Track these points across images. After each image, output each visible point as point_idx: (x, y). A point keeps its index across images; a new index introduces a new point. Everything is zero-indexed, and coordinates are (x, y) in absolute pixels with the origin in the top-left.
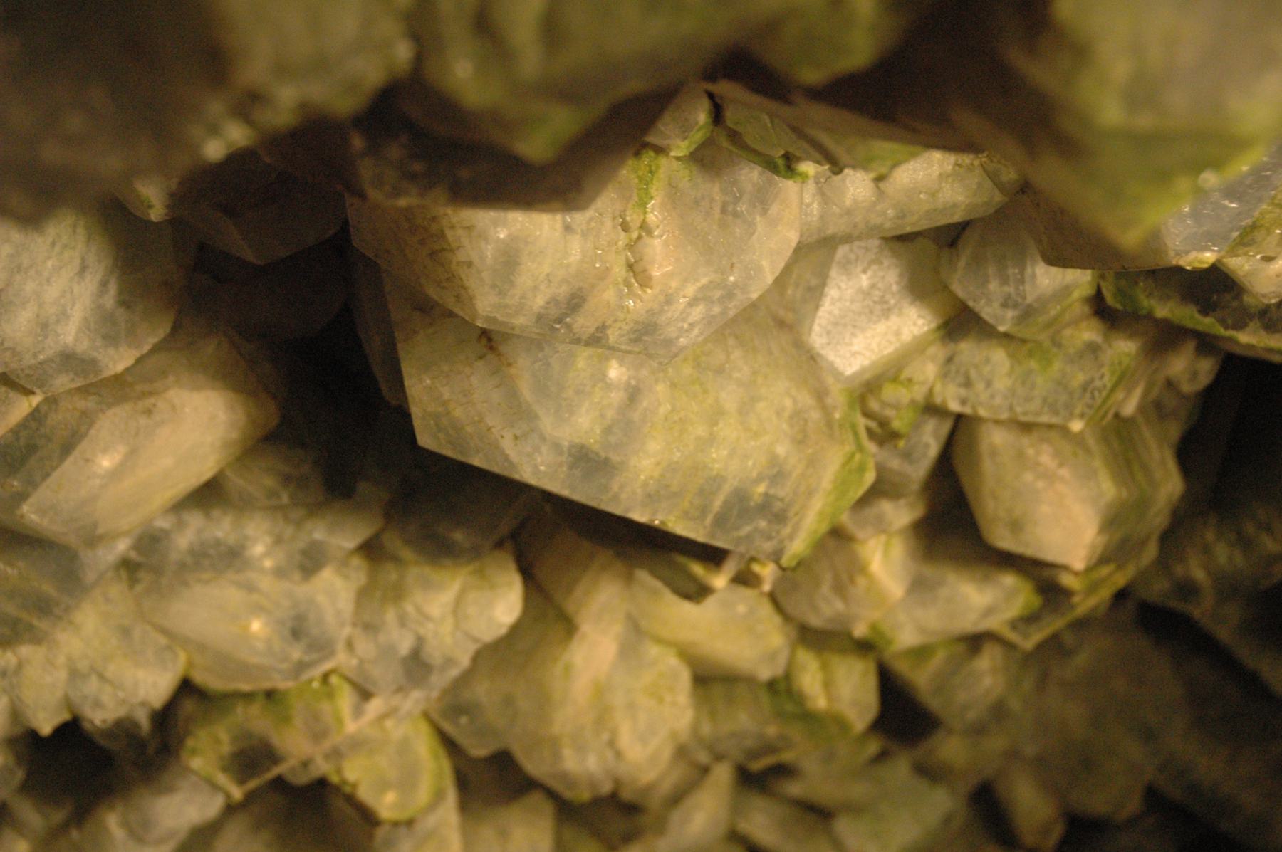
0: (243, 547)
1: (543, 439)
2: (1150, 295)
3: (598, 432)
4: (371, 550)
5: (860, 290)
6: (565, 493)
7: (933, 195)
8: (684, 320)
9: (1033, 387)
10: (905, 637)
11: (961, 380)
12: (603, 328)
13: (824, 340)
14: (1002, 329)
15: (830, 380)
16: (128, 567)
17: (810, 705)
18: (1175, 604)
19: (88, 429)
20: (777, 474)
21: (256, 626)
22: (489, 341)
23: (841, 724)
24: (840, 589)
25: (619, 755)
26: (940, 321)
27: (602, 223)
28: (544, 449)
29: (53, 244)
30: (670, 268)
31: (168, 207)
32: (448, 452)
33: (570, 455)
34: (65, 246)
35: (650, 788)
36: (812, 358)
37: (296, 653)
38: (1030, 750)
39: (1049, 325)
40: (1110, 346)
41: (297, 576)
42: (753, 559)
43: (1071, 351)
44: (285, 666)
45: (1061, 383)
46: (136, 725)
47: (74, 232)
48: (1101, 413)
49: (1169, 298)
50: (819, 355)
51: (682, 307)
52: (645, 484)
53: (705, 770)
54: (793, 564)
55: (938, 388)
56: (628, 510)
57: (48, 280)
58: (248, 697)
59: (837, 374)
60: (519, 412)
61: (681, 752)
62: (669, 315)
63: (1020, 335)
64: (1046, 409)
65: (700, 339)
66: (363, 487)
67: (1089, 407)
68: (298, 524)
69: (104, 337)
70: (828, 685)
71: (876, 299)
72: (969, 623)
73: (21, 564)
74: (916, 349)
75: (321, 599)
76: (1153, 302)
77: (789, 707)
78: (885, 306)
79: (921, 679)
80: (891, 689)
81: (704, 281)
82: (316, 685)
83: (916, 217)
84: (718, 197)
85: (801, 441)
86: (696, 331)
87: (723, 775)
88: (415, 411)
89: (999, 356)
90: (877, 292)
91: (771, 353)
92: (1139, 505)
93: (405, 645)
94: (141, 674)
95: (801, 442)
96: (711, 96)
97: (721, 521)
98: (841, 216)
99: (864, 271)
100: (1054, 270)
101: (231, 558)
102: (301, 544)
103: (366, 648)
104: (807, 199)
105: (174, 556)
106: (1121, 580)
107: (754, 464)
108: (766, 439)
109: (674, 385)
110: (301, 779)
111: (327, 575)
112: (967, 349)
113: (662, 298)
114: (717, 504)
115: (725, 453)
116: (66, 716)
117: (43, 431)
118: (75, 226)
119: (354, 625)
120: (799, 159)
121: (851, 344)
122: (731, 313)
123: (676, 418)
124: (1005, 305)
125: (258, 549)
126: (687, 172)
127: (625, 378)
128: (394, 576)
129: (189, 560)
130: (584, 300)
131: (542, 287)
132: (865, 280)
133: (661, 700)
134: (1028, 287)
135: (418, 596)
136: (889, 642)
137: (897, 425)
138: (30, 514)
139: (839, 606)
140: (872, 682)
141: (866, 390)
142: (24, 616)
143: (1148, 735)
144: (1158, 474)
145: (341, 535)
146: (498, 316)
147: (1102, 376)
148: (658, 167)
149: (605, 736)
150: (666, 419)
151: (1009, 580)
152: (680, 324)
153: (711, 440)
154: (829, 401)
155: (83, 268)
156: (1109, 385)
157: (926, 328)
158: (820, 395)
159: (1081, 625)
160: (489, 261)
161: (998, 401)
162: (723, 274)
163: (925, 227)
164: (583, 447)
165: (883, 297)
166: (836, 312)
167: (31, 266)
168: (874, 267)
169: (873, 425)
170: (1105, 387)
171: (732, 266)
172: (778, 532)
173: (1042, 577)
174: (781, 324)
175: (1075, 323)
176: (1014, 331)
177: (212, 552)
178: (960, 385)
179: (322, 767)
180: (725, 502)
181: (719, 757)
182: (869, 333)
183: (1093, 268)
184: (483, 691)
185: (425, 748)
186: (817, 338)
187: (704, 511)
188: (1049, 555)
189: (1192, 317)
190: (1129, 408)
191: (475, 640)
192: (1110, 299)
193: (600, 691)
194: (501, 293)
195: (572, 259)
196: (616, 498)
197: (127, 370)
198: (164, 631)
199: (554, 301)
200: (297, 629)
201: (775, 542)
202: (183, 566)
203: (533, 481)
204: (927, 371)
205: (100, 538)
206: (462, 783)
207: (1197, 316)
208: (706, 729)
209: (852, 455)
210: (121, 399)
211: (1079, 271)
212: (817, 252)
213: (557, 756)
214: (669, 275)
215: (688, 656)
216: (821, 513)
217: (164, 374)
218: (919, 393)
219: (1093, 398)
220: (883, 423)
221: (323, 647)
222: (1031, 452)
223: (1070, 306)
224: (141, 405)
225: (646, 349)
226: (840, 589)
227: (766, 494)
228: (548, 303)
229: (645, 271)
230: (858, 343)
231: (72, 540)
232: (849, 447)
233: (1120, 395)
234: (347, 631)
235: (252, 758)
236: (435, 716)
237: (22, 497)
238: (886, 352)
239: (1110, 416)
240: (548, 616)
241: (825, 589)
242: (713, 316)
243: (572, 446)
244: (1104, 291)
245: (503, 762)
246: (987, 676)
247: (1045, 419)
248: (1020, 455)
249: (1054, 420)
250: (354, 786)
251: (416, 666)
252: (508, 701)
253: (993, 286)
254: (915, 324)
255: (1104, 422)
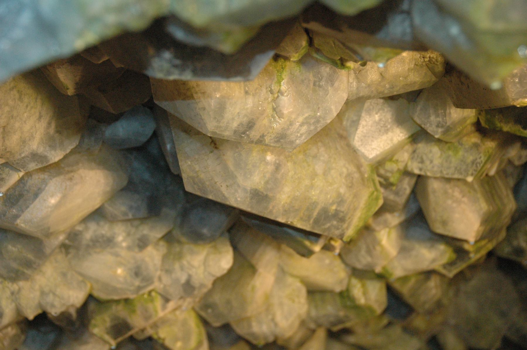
0: (113, 237)
1: (239, 186)
2: (501, 121)
3: (263, 183)
4: (168, 238)
5: (375, 122)
6: (249, 210)
7: (406, 78)
8: (298, 132)
9: (451, 162)
10: (397, 272)
11: (419, 160)
12: (263, 136)
13: (360, 143)
14: (437, 136)
15: (363, 160)
16: (65, 247)
17: (358, 302)
18: (513, 257)
19: (45, 187)
20: (341, 201)
21: (119, 271)
22: (214, 143)
23: (370, 309)
24: (369, 252)
25: (276, 325)
26: (410, 134)
27: (262, 90)
28: (239, 191)
29: (27, 106)
30: (291, 110)
31: (75, 89)
32: (198, 193)
33: (251, 193)
34: (32, 108)
35: (290, 338)
36: (355, 151)
37: (137, 283)
38: (453, 322)
39: (456, 136)
40: (484, 145)
41: (137, 250)
42: (331, 239)
43: (467, 147)
44: (132, 288)
45: (463, 161)
46: (70, 315)
47: (36, 101)
48: (481, 172)
49: (509, 122)
50: (358, 150)
51: (297, 126)
52: (284, 206)
53: (313, 331)
54: (348, 240)
55: (409, 164)
56: (276, 217)
57: (25, 122)
58: (117, 302)
59: (365, 157)
60: (229, 176)
61: (303, 323)
62: (292, 130)
63: (444, 140)
64: (456, 172)
65: (305, 141)
66: (165, 210)
67: (475, 171)
68: (137, 227)
69: (50, 146)
70: (365, 293)
71: (382, 125)
72: (425, 265)
73: (19, 246)
74: (400, 147)
75: (147, 259)
76: (502, 124)
77: (349, 303)
78: (386, 128)
79: (405, 290)
80: (392, 292)
81: (307, 115)
82: (146, 296)
83: (398, 88)
84: (312, 78)
85: (350, 187)
86: (303, 137)
87: (321, 334)
88: (184, 176)
89: (435, 150)
90: (382, 122)
91: (337, 149)
92: (498, 213)
93: (183, 279)
94: (71, 293)
95: (351, 187)
96: (307, 31)
97: (317, 222)
98: (366, 88)
99: (377, 114)
100: (459, 110)
101: (108, 242)
102: (138, 236)
103: (166, 280)
104: (351, 80)
105: (84, 242)
106: (490, 246)
107: (330, 197)
108: (335, 186)
109: (295, 163)
110: (141, 337)
111: (150, 249)
112: (422, 147)
113: (288, 123)
114: (315, 214)
115: (318, 192)
116: (40, 311)
117: (25, 188)
118: (36, 99)
119: (162, 270)
120: (347, 61)
121: (371, 145)
122: (319, 129)
123: (296, 177)
124: (438, 126)
125: (120, 238)
126: (298, 68)
127: (274, 160)
128: (178, 249)
129: (91, 244)
130: (254, 124)
131: (236, 118)
132: (377, 117)
133: (293, 301)
134: (447, 118)
135: (188, 257)
136: (391, 275)
137: (392, 180)
138: (21, 223)
139: (369, 259)
140: (384, 292)
141: (378, 165)
142: (21, 268)
143: (503, 315)
144: (506, 201)
145: (155, 232)
146: (217, 131)
147: (480, 158)
148: (285, 66)
149: (270, 317)
150: (292, 177)
151: (442, 247)
152: (296, 134)
153: (312, 186)
154: (363, 169)
155: (40, 117)
156: (483, 161)
157: (404, 138)
158: (359, 167)
159: (473, 267)
160: (213, 107)
161: (435, 169)
162: (315, 112)
163: (402, 92)
164: (256, 190)
165: (385, 124)
166: (365, 131)
167: (18, 116)
168: (381, 112)
169: (382, 180)
170: (482, 162)
171: (319, 108)
172: (342, 226)
173: (456, 245)
174: (341, 137)
175: (468, 135)
176: (442, 138)
177: (100, 240)
178: (419, 163)
179: (150, 332)
180: (318, 213)
181: (319, 326)
182: (379, 140)
183: (476, 108)
184: (217, 298)
185: (193, 323)
186: (356, 142)
187: (309, 217)
188: (460, 235)
189: (519, 130)
190: (492, 172)
191: (213, 276)
192: (483, 124)
193: (268, 297)
194: (218, 121)
195: (249, 106)
196: (271, 212)
197: (60, 161)
198: (81, 274)
199: (241, 124)
200: (137, 272)
201: (340, 230)
202: (88, 246)
203: (235, 205)
204: (404, 156)
205: (52, 234)
206: (211, 339)
207: (521, 130)
208: (314, 313)
209: (373, 193)
210: (59, 174)
211: (470, 110)
212: (355, 104)
213: (250, 326)
214: (292, 113)
215: (304, 281)
216: (360, 218)
217: (77, 163)
218: (401, 166)
219: (477, 166)
220: (386, 179)
221: (148, 280)
222: (450, 191)
223: (466, 127)
224: (68, 176)
225: (282, 145)
226: (369, 252)
227: (336, 210)
228: (239, 125)
229: (280, 111)
230: (375, 144)
231: (39, 235)
232: (372, 189)
233: (488, 166)
234: (158, 273)
235: (119, 328)
236: (197, 309)
237: (17, 217)
238: (386, 148)
239: (484, 175)
240: (244, 266)
241: (363, 252)
242: (311, 131)
243: (251, 190)
244: (481, 120)
245: (227, 327)
246: (433, 289)
247: (456, 176)
248: (446, 192)
249: (460, 177)
250: (164, 340)
251: (188, 287)
252: (228, 302)
253: (432, 118)
254: (399, 136)
255: (482, 178)
